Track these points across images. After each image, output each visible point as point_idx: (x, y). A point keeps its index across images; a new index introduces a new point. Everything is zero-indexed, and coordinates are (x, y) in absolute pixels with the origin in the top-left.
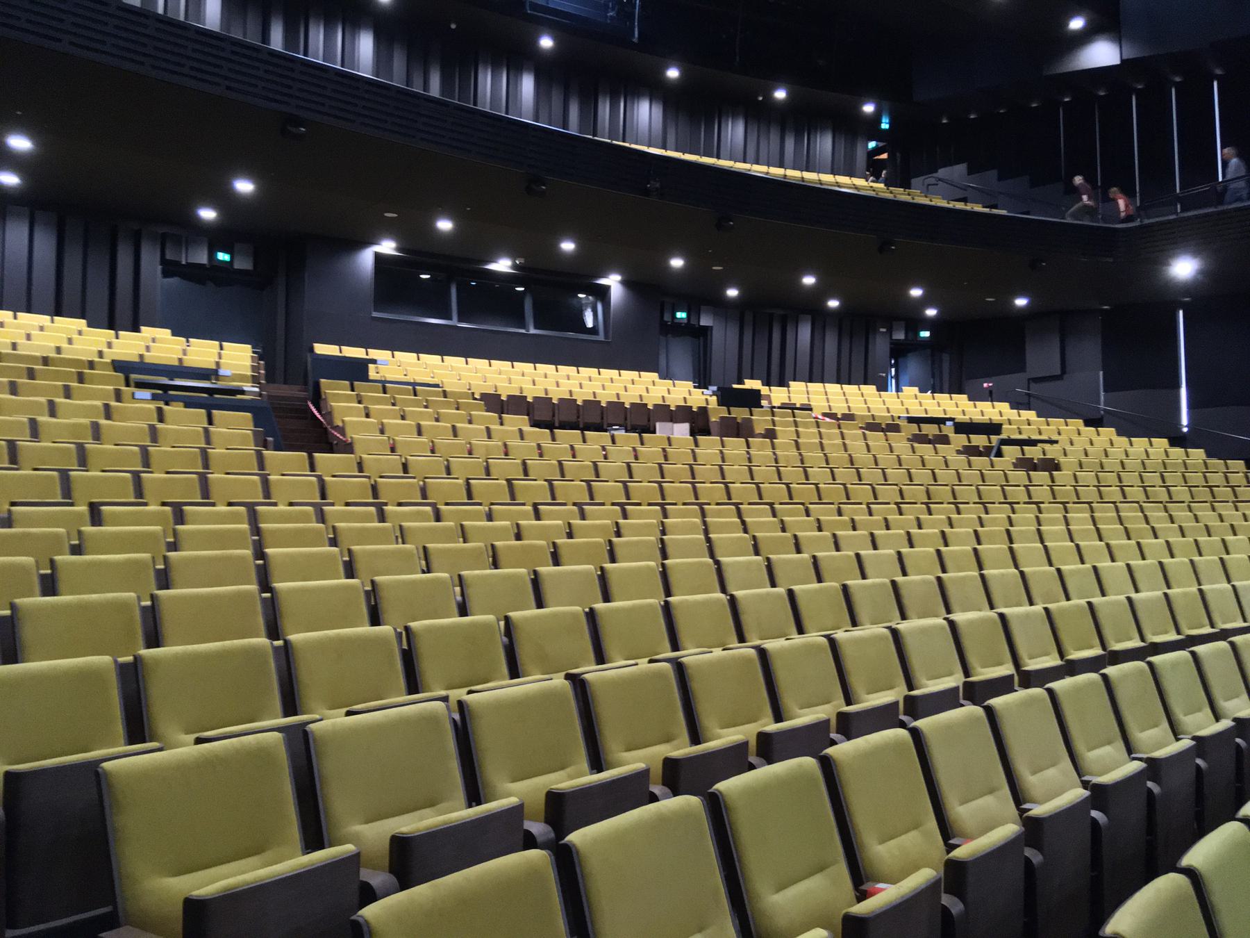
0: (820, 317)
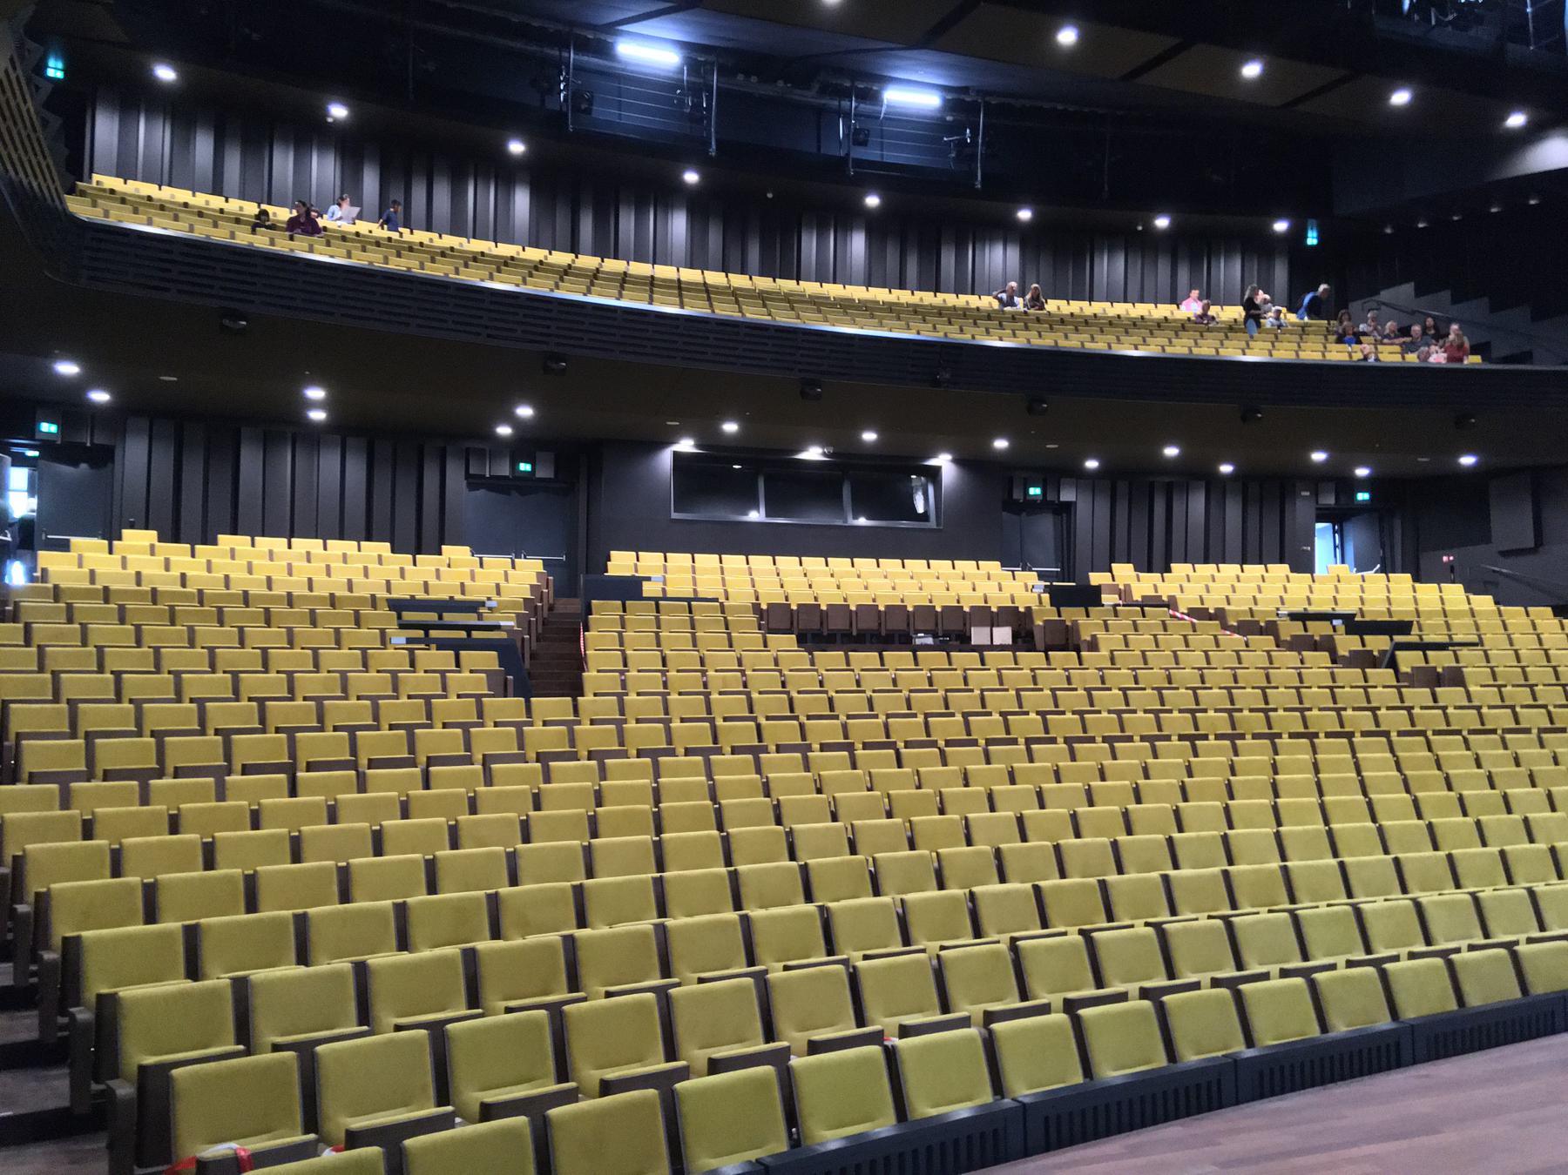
0: (1216, 487)
